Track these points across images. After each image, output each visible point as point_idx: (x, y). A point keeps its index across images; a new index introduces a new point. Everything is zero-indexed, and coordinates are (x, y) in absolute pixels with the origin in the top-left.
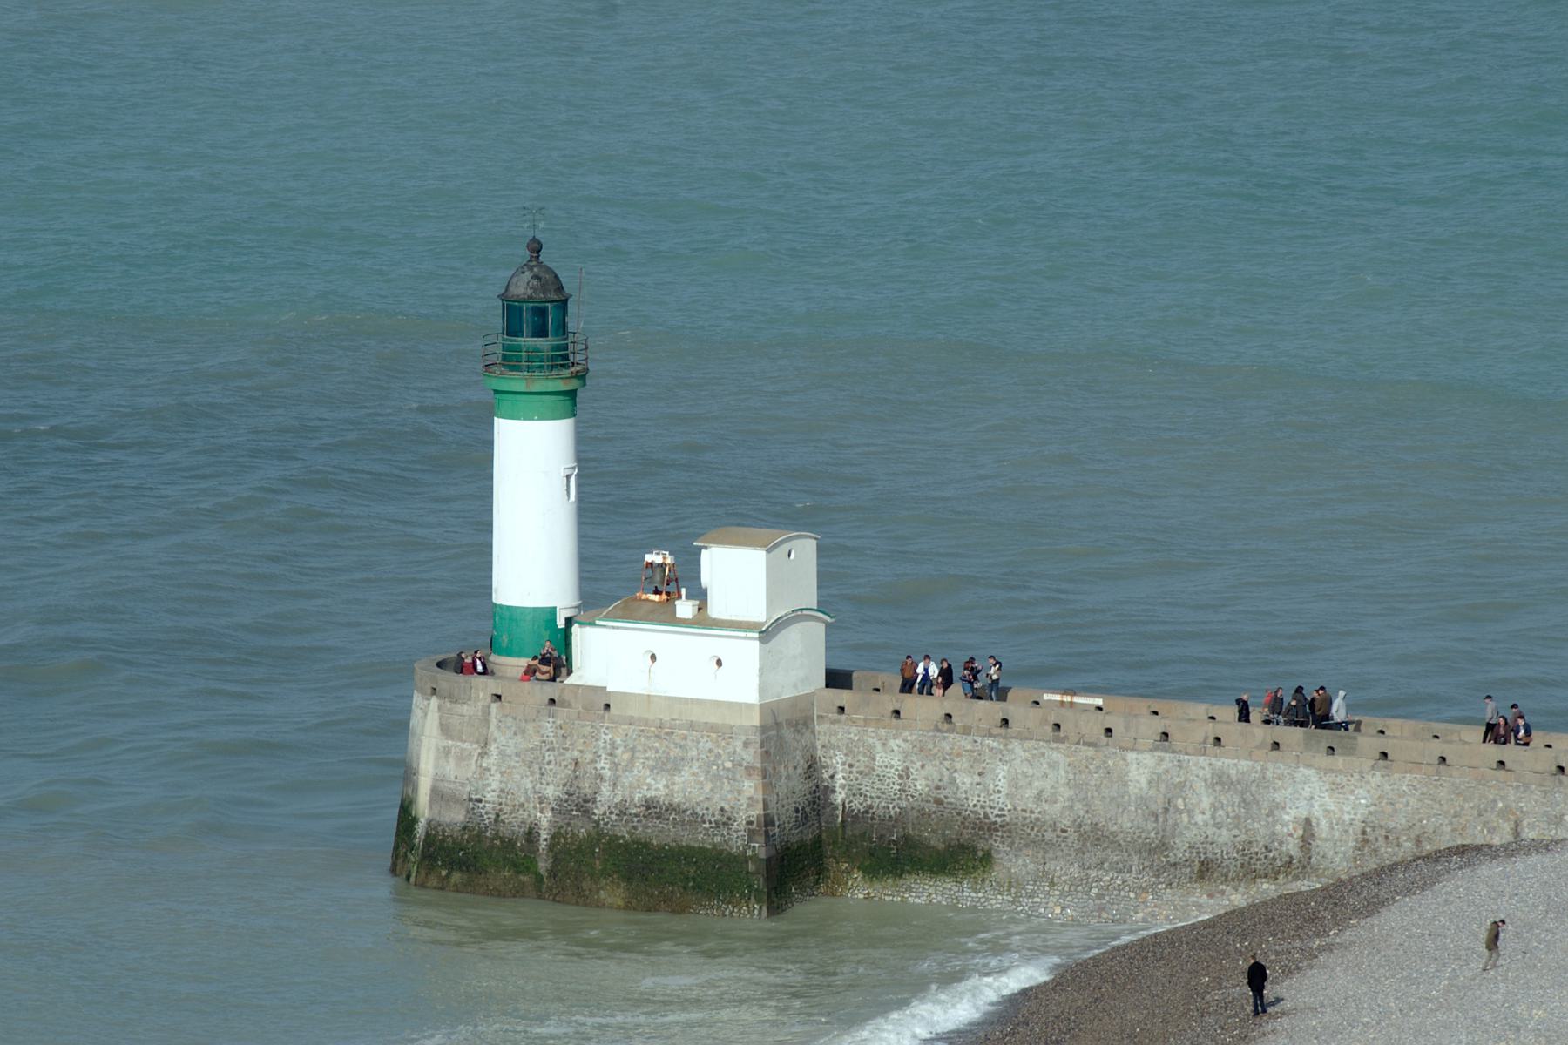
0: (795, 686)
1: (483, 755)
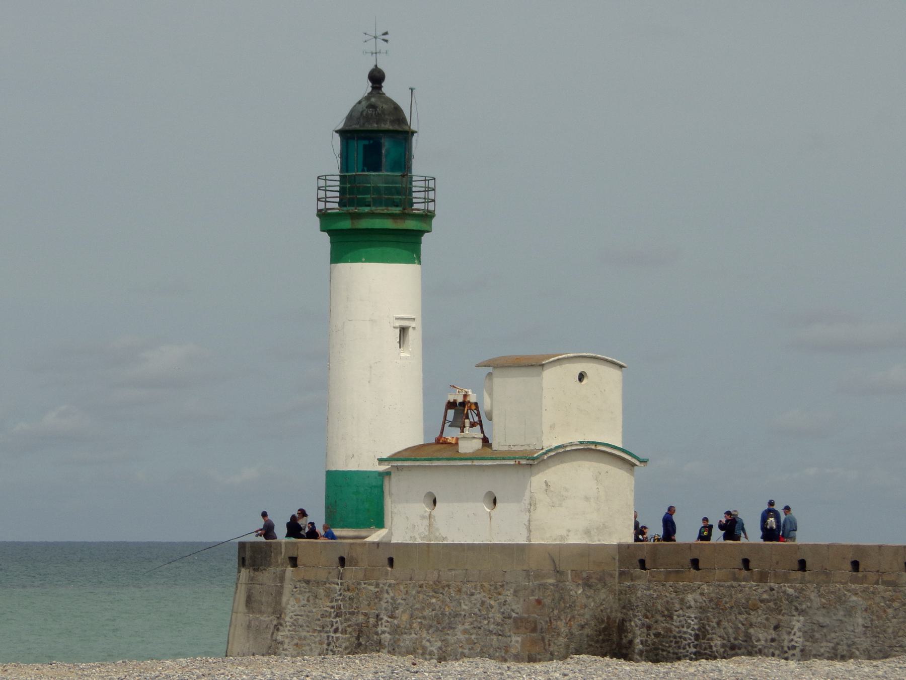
0: (587, 532)
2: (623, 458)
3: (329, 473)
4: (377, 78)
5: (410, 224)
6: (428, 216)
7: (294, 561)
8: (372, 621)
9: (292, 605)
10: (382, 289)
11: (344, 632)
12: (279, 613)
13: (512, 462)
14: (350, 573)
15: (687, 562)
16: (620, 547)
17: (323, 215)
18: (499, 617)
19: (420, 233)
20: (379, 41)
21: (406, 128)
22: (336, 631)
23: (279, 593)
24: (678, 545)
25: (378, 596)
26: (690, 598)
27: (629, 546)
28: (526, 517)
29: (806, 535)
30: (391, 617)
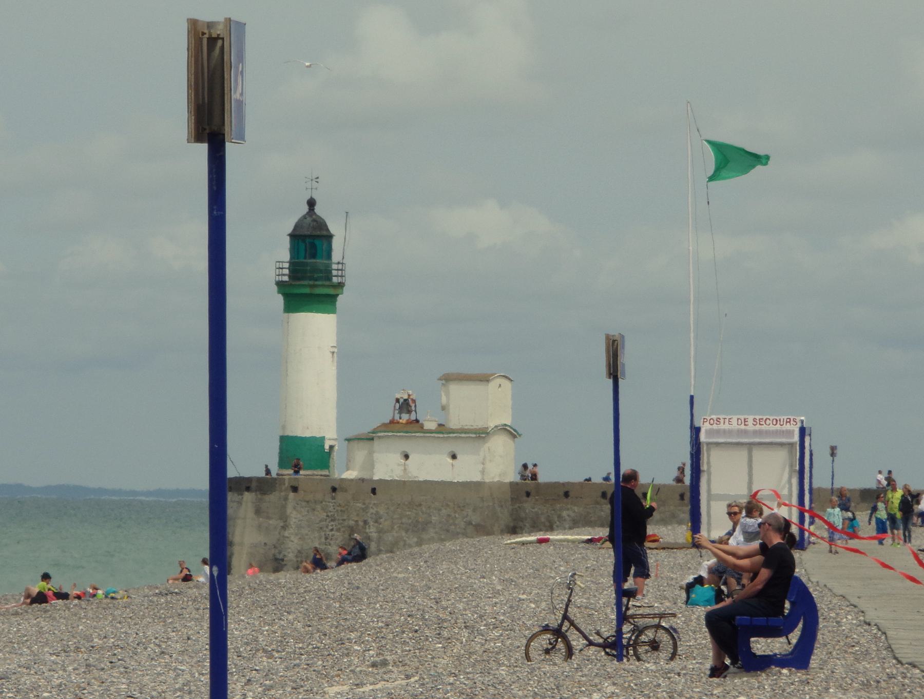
1: (284, 528)
2: (512, 433)
3: (284, 440)
4: (311, 203)
5: (331, 291)
6: (341, 285)
7: (295, 489)
8: (361, 523)
9: (294, 516)
10: (317, 329)
11: (338, 530)
12: (284, 518)
13: (474, 436)
14: (339, 496)
15: (562, 493)
16: (511, 484)
17: (280, 284)
18: (463, 525)
19: (337, 295)
20: (314, 182)
21: (325, 233)
22: (332, 530)
23: (284, 507)
24: (539, 484)
25: (365, 510)
26: (565, 514)
27: (517, 484)
28: (480, 467)
29: (542, 479)
30: (376, 522)
